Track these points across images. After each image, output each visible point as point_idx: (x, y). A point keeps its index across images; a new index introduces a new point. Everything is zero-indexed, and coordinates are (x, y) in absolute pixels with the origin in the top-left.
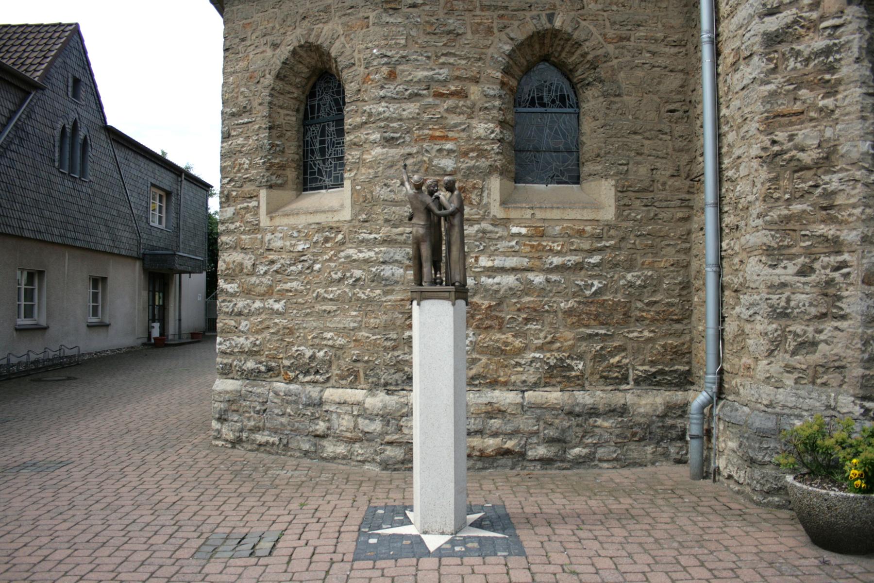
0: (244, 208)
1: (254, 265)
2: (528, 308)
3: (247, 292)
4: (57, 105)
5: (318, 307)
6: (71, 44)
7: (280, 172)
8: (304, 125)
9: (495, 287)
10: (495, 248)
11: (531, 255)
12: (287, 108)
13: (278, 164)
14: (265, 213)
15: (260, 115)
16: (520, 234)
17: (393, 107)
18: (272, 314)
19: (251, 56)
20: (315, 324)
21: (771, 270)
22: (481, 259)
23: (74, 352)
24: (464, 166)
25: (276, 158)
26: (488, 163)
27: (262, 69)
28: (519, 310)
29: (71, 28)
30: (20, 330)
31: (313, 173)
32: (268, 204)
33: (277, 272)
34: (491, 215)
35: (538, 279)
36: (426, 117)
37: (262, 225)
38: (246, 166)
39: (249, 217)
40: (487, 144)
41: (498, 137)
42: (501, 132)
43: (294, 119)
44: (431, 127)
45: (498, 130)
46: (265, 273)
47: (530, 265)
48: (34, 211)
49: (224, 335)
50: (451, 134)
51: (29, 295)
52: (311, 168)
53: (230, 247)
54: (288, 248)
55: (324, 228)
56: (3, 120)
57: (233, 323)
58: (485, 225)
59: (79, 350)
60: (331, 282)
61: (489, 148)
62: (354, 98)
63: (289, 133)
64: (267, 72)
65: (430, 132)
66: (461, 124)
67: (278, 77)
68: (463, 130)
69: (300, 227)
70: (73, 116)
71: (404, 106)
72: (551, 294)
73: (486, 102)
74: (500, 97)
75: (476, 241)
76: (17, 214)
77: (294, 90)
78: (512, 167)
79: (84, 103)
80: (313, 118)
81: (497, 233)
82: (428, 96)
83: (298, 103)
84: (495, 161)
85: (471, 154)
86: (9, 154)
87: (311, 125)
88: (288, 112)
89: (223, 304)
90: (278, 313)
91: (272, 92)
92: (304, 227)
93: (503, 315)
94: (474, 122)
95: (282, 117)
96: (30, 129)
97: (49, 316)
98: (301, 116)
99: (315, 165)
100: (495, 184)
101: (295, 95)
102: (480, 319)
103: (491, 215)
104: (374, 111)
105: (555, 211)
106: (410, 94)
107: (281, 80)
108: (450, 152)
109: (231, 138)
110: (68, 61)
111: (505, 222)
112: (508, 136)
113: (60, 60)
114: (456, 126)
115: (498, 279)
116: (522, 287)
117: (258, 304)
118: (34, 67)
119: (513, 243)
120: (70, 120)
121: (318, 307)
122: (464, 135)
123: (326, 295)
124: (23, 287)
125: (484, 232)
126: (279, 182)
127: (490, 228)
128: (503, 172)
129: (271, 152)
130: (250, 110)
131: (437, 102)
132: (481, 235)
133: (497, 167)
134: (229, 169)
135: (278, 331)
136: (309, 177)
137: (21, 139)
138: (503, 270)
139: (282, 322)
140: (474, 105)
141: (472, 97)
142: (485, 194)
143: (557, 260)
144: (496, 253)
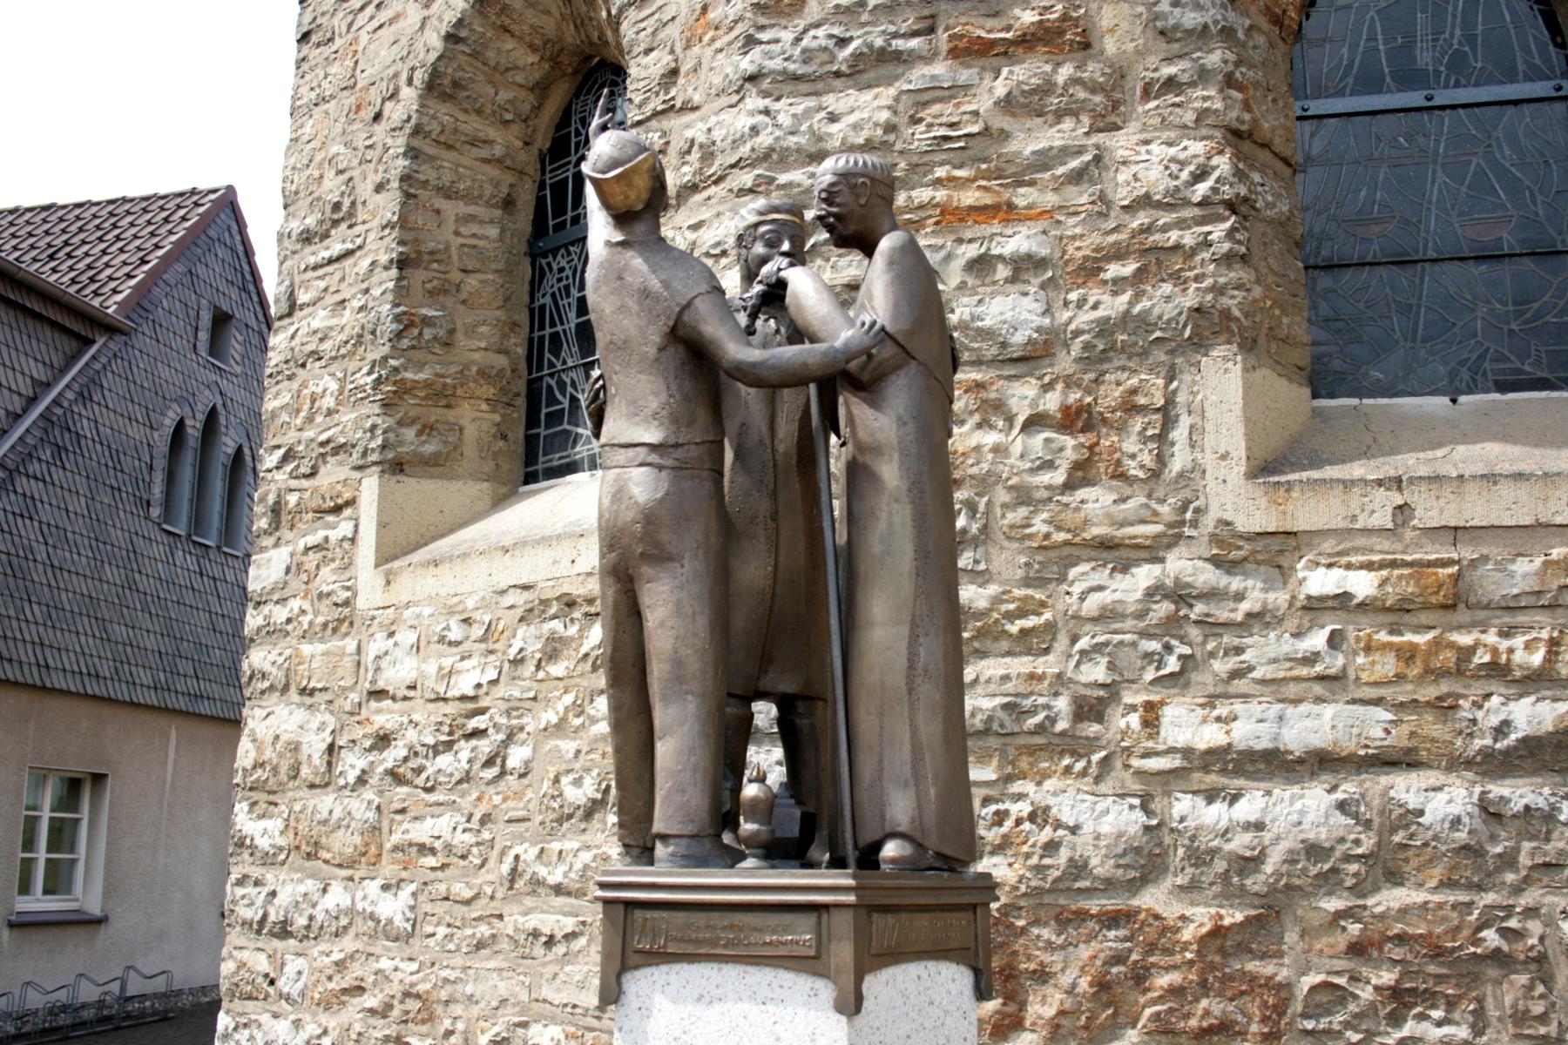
0: (317, 548)
1: (331, 749)
2: (1401, 939)
3: (308, 850)
4: (165, 373)
5: (517, 919)
6: (212, 233)
7: (435, 414)
8: (534, 255)
9: (1240, 843)
10: (1232, 663)
11: (1403, 693)
12: (468, 198)
13: (427, 384)
14: (372, 558)
15: (376, 223)
16: (1345, 596)
17: (786, 110)
18: (373, 936)
19: (364, 38)
20: (503, 988)
21: (424, 795)
22: (1169, 713)
23: (159, 985)
24: (1085, 318)
25: (421, 366)
26: (1189, 300)
27: (391, 72)
28: (1357, 949)
29: (212, 197)
30: (23, 925)
31: (556, 418)
32: (382, 526)
33: (395, 776)
34: (1209, 523)
35: (1443, 801)
36: (920, 137)
37: (361, 603)
38: (328, 402)
39: (327, 579)
40: (1181, 224)
41: (1227, 192)
42: (1239, 174)
43: (493, 232)
44: (940, 172)
45: (1223, 164)
46: (362, 780)
47: (1399, 738)
48: (84, 624)
49: (238, 1005)
50: (1023, 197)
51: (62, 835)
52: (553, 400)
53: (272, 688)
54: (430, 683)
55: (545, 603)
56: (17, 404)
57: (261, 964)
58: (1180, 565)
59: (169, 982)
60: (560, 820)
61: (1189, 239)
62: (656, 104)
63: (472, 281)
64: (404, 77)
65: (941, 195)
66: (1065, 153)
67: (437, 86)
68: (1077, 177)
69: (470, 604)
70: (206, 399)
71: (831, 102)
72: (1510, 877)
73: (1168, 60)
74: (1227, 33)
75: (1146, 634)
76: (31, 633)
77: (492, 133)
78: (1296, 325)
79: (238, 369)
80: (560, 227)
81: (1239, 597)
82: (929, 58)
83: (509, 178)
84: (1219, 290)
85: (1114, 270)
86: (22, 483)
87: (555, 252)
88: (472, 209)
89: (240, 891)
90: (383, 931)
91: (416, 143)
92: (483, 605)
93: (1283, 975)
94: (1121, 143)
95: (450, 226)
96: (85, 427)
97: (108, 892)
98: (523, 220)
99: (562, 385)
100: (1221, 388)
101: (498, 151)
102: (1175, 991)
103: (1209, 523)
104: (717, 135)
105: (1505, 490)
106: (857, 56)
107: (445, 97)
108: (1023, 266)
109: (298, 314)
110: (201, 270)
111: (1276, 551)
112: (1272, 200)
113: (179, 267)
114: (1045, 160)
115: (1251, 806)
116: (1368, 843)
117: (337, 897)
118: (113, 285)
119: (1317, 640)
120: (200, 407)
121: (517, 919)
122: (1081, 197)
123: (542, 871)
124: (46, 814)
125: (1180, 595)
126: (429, 448)
127: (1208, 576)
128: (1254, 342)
129: (405, 343)
130: (351, 213)
131: (965, 75)
132: (1164, 608)
133: (1226, 314)
134: (285, 417)
135: (389, 1007)
136: (542, 431)
137: (59, 449)
138: (1273, 764)
139: (398, 967)
140: (1119, 75)
141: (1110, 46)
142: (1179, 434)
143: (1531, 715)
144: (1240, 685)
